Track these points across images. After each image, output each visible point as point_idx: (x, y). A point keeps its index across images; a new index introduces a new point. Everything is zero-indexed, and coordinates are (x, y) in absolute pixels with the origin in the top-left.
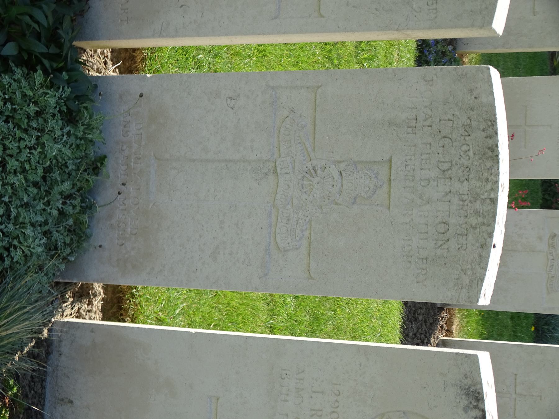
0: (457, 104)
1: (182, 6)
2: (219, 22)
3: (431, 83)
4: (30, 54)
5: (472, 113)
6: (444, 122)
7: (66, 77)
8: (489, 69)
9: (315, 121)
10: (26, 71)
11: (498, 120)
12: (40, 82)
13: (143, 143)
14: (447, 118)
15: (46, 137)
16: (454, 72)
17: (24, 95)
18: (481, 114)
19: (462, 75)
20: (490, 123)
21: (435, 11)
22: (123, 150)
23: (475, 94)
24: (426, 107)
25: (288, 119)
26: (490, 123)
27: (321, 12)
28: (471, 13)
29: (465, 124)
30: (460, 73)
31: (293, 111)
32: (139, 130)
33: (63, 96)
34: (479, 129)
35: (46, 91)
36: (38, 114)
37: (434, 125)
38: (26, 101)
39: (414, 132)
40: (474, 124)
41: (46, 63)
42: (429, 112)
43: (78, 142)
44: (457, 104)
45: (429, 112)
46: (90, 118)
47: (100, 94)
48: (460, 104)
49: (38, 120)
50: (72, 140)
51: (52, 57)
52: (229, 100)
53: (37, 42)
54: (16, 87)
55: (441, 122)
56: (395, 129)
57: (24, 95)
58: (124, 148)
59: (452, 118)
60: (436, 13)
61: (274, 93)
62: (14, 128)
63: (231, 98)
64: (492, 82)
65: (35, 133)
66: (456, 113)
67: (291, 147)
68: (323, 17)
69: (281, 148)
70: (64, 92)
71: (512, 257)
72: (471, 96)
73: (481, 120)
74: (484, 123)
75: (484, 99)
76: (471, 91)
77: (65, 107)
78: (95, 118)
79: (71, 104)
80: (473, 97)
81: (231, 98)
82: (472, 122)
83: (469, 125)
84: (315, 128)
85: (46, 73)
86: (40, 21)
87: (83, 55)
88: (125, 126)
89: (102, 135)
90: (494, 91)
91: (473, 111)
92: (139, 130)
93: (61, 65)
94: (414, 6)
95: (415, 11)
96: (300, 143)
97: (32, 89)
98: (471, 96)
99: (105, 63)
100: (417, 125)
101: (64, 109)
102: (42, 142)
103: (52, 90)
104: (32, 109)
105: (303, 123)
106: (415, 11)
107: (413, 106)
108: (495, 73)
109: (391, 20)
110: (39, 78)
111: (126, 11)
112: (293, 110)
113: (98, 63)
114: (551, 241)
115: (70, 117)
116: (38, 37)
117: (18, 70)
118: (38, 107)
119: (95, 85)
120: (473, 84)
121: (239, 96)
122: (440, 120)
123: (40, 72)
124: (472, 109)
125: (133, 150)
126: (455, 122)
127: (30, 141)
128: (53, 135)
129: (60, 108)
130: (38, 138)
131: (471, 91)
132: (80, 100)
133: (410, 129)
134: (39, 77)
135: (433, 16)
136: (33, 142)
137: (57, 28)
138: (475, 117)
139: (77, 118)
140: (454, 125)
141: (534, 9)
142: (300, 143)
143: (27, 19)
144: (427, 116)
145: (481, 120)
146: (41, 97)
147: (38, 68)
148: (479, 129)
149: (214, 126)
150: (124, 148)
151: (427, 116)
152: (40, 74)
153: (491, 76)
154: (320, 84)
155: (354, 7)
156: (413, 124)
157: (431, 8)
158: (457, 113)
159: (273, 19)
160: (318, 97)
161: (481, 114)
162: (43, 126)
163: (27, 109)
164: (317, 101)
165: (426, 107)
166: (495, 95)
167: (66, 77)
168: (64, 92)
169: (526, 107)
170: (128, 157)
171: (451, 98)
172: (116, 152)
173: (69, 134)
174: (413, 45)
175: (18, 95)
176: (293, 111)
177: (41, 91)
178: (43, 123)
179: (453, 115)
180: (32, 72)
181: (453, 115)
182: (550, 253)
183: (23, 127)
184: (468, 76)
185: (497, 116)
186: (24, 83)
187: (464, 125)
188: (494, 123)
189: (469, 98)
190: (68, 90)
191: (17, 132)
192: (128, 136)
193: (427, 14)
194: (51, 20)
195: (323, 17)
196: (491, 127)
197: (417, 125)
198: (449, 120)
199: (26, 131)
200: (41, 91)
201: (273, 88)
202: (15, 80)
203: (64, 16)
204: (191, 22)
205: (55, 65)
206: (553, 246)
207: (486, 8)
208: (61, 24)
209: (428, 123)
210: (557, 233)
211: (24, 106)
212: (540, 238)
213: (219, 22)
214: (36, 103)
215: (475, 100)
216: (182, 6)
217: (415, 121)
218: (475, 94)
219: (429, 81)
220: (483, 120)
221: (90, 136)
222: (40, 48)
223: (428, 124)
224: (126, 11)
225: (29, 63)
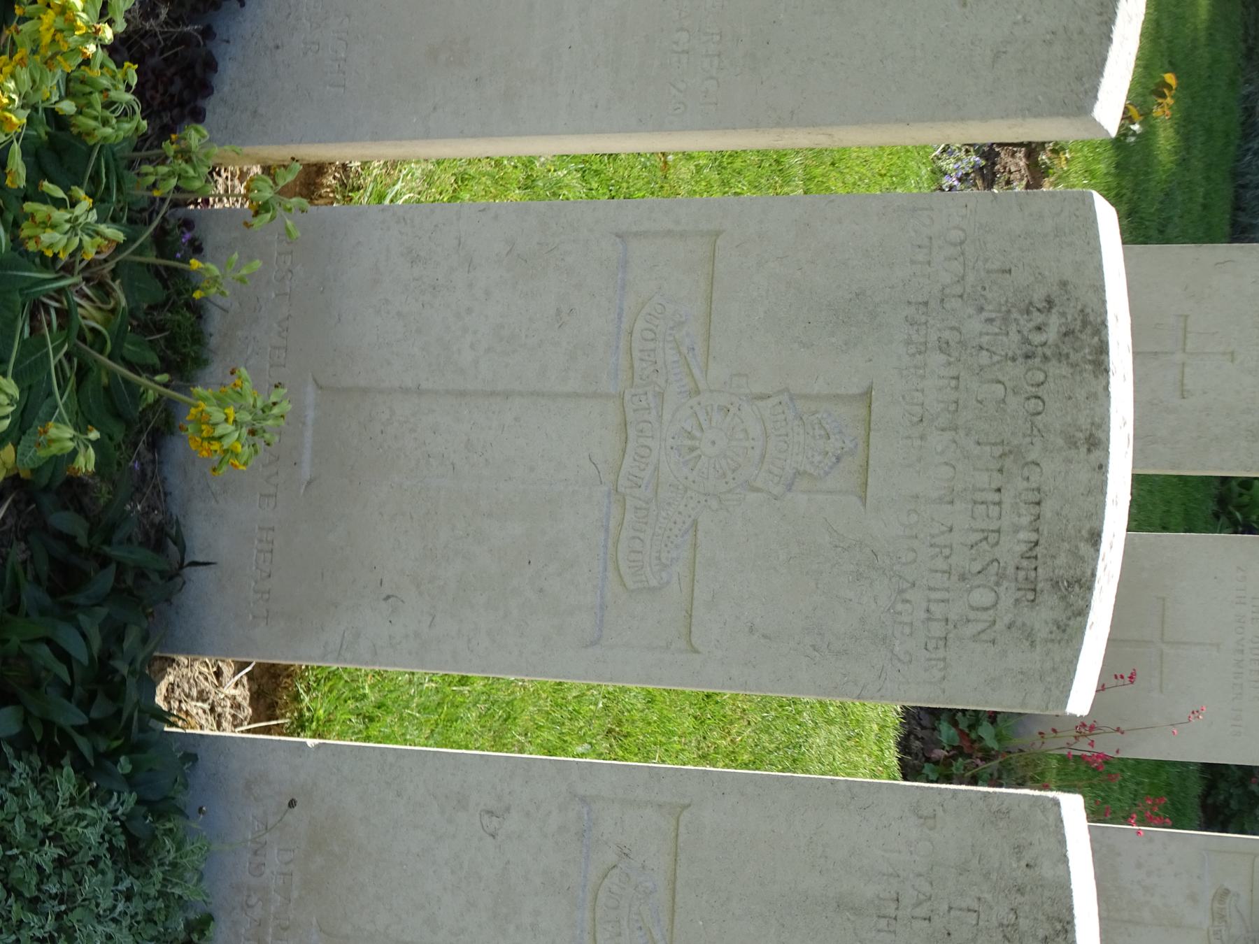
0: (987, 876)
1: (388, 597)
2: (469, 641)
3: (930, 822)
4: (48, 725)
5: (1020, 899)
6: (959, 913)
7: (128, 768)
8: (1056, 803)
9: (674, 883)
10: (37, 762)
11: (1076, 921)
12: (67, 795)
13: (295, 894)
14: (964, 905)
15: (78, 913)
16: (981, 803)
17: (31, 825)
18: (1039, 902)
19: (999, 811)
20: (1059, 927)
21: (942, 665)
22: (249, 906)
23: (1027, 857)
24: (920, 875)
25: (616, 871)
26: (1059, 927)
27: (693, 640)
28: (1021, 677)
29: (1005, 922)
30: (994, 808)
31: (627, 855)
32: (287, 863)
33: (119, 812)
34: (1035, 936)
35: (80, 810)
36: (60, 863)
37: (935, 918)
38: (35, 836)
39: (892, 929)
40: (1024, 924)
41: (83, 744)
42: (926, 888)
43: (150, 905)
44: (987, 876)
45: (926, 888)
46: (177, 850)
47: (201, 809)
48: (994, 876)
49: (61, 876)
50: (137, 906)
51: (94, 728)
52: (486, 818)
53: (65, 702)
54: (15, 808)
55: (952, 912)
56: (852, 918)
57: (31, 825)
58: (253, 900)
59: (975, 905)
60: (945, 668)
61: (585, 810)
62: (6, 900)
63: (491, 813)
64: (1063, 835)
65: (53, 907)
66: (986, 895)
67: (620, 934)
68: (696, 651)
69: (598, 935)
70: (122, 804)
71: (1129, 936)
72: (1019, 860)
73: (1040, 917)
74: (1046, 925)
75: (1047, 870)
76: (1018, 850)
77: (123, 838)
78: (188, 847)
79: (138, 828)
80: (1023, 864)
81: (491, 813)
82: (1021, 920)
83: (1014, 926)
84: (674, 899)
85: (81, 766)
86: (73, 653)
87: (169, 670)
88: (255, 853)
89: (204, 885)
90: (1071, 855)
91: (1023, 894)
92: (287, 863)
93: (116, 744)
94: (897, 649)
95: (899, 660)
96: (641, 928)
97: (49, 807)
98: (1019, 860)
99: (218, 674)
100: (900, 913)
101: (121, 842)
102: (69, 924)
103: (95, 805)
104: (52, 851)
105: (648, 884)
106: (899, 660)
107: (891, 870)
108: (1073, 806)
109: (845, 675)
110: (65, 785)
111: (266, 596)
112: (626, 851)
113: (200, 697)
114: (1216, 905)
115: (133, 852)
116: (68, 693)
117: (20, 767)
118: (62, 847)
119: (191, 752)
120: (1024, 835)
121: (508, 809)
122: (950, 908)
123: (68, 770)
124: (1020, 891)
125: (273, 909)
126: (982, 916)
127: (42, 927)
128: (93, 906)
129: (110, 842)
130: (59, 916)
131: (1018, 850)
132: (153, 784)
133: (883, 923)
134: (66, 781)
135: (939, 675)
136: (47, 928)
137: (111, 656)
138: (1027, 908)
139: (150, 853)
140: (981, 923)
141: (1182, 385)
142: (641, 928)
143: (45, 650)
144: (922, 897)
145: (1040, 917)
146: (70, 824)
147: (66, 761)
148: (1035, 936)
149: (453, 872)
150: (253, 900)
151: (922, 897)
152: (68, 776)
153: (1062, 821)
154: (687, 801)
155: (765, 636)
156: (891, 911)
157: (933, 656)
158: (988, 897)
159: (586, 646)
160: (682, 829)
161: (1039, 902)
162: (72, 890)
163: (37, 858)
164: (681, 839)
165: (920, 875)
166: (1070, 864)
167: (128, 768)
168: (122, 804)
169: (1164, 599)
170: (261, 923)
171: (975, 861)
172: (234, 908)
173: (129, 896)
174: (894, 719)
175: (19, 828)
176: (627, 855)
177: (70, 812)
178: (72, 881)
179: (979, 899)
180: (50, 768)
181: (979, 899)
182: (1215, 933)
183: (27, 895)
184: (1012, 814)
185: (1076, 912)
186: (33, 798)
187: (1001, 925)
188: (1068, 927)
189: (1015, 865)
190: (131, 799)
191: (14, 908)
192: (261, 875)
193: (926, 670)
194: (96, 643)
195: (696, 651)
196: (1062, 936)
197: (900, 913)
198: (969, 910)
199: (34, 904)
200: (70, 812)
201: (583, 800)
202: (12, 790)
203: (125, 625)
204: (407, 636)
205: (103, 746)
206: (1222, 917)
207: (1054, 669)
208: (120, 639)
209: (922, 911)
210: (1230, 888)
211: (31, 849)
212: (1193, 898)
213: (469, 641)
214: (56, 839)
215: (1028, 871)
216: (388, 597)
217: (894, 905)
218: (1027, 857)
219: (926, 818)
220: (1044, 918)
221: (177, 891)
222: (70, 716)
223: (923, 915)
224: (266, 596)
225: (49, 747)
